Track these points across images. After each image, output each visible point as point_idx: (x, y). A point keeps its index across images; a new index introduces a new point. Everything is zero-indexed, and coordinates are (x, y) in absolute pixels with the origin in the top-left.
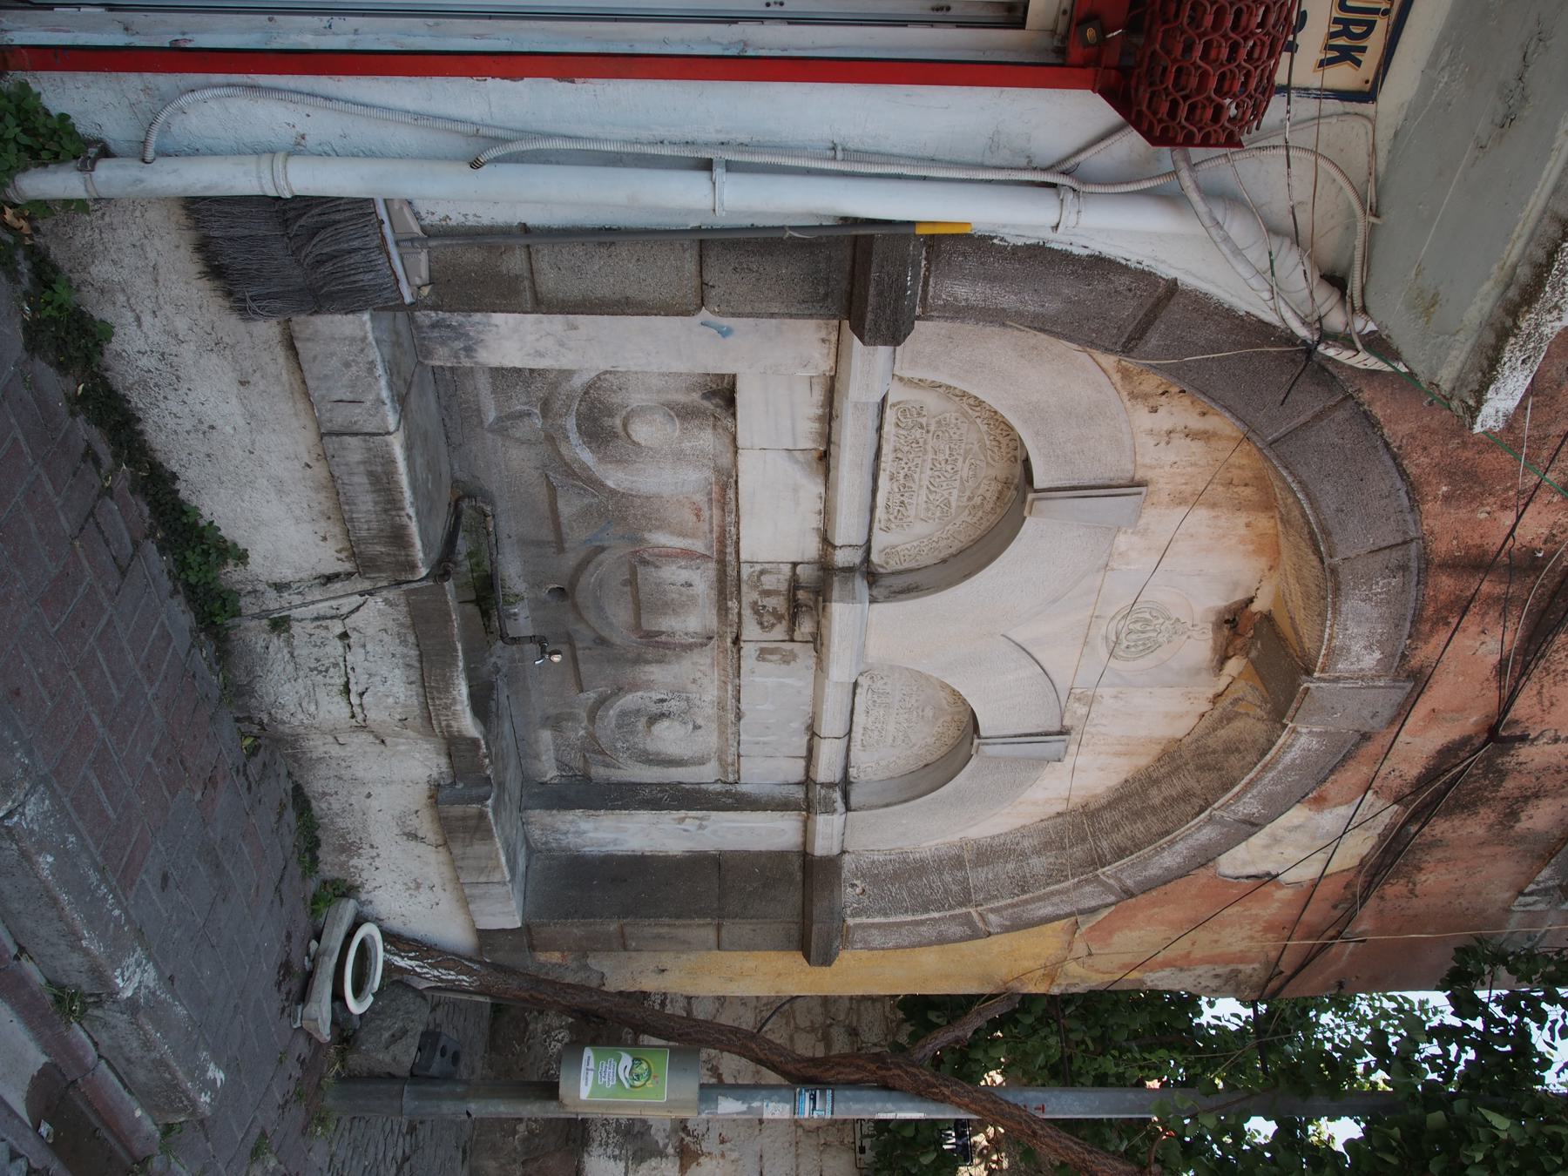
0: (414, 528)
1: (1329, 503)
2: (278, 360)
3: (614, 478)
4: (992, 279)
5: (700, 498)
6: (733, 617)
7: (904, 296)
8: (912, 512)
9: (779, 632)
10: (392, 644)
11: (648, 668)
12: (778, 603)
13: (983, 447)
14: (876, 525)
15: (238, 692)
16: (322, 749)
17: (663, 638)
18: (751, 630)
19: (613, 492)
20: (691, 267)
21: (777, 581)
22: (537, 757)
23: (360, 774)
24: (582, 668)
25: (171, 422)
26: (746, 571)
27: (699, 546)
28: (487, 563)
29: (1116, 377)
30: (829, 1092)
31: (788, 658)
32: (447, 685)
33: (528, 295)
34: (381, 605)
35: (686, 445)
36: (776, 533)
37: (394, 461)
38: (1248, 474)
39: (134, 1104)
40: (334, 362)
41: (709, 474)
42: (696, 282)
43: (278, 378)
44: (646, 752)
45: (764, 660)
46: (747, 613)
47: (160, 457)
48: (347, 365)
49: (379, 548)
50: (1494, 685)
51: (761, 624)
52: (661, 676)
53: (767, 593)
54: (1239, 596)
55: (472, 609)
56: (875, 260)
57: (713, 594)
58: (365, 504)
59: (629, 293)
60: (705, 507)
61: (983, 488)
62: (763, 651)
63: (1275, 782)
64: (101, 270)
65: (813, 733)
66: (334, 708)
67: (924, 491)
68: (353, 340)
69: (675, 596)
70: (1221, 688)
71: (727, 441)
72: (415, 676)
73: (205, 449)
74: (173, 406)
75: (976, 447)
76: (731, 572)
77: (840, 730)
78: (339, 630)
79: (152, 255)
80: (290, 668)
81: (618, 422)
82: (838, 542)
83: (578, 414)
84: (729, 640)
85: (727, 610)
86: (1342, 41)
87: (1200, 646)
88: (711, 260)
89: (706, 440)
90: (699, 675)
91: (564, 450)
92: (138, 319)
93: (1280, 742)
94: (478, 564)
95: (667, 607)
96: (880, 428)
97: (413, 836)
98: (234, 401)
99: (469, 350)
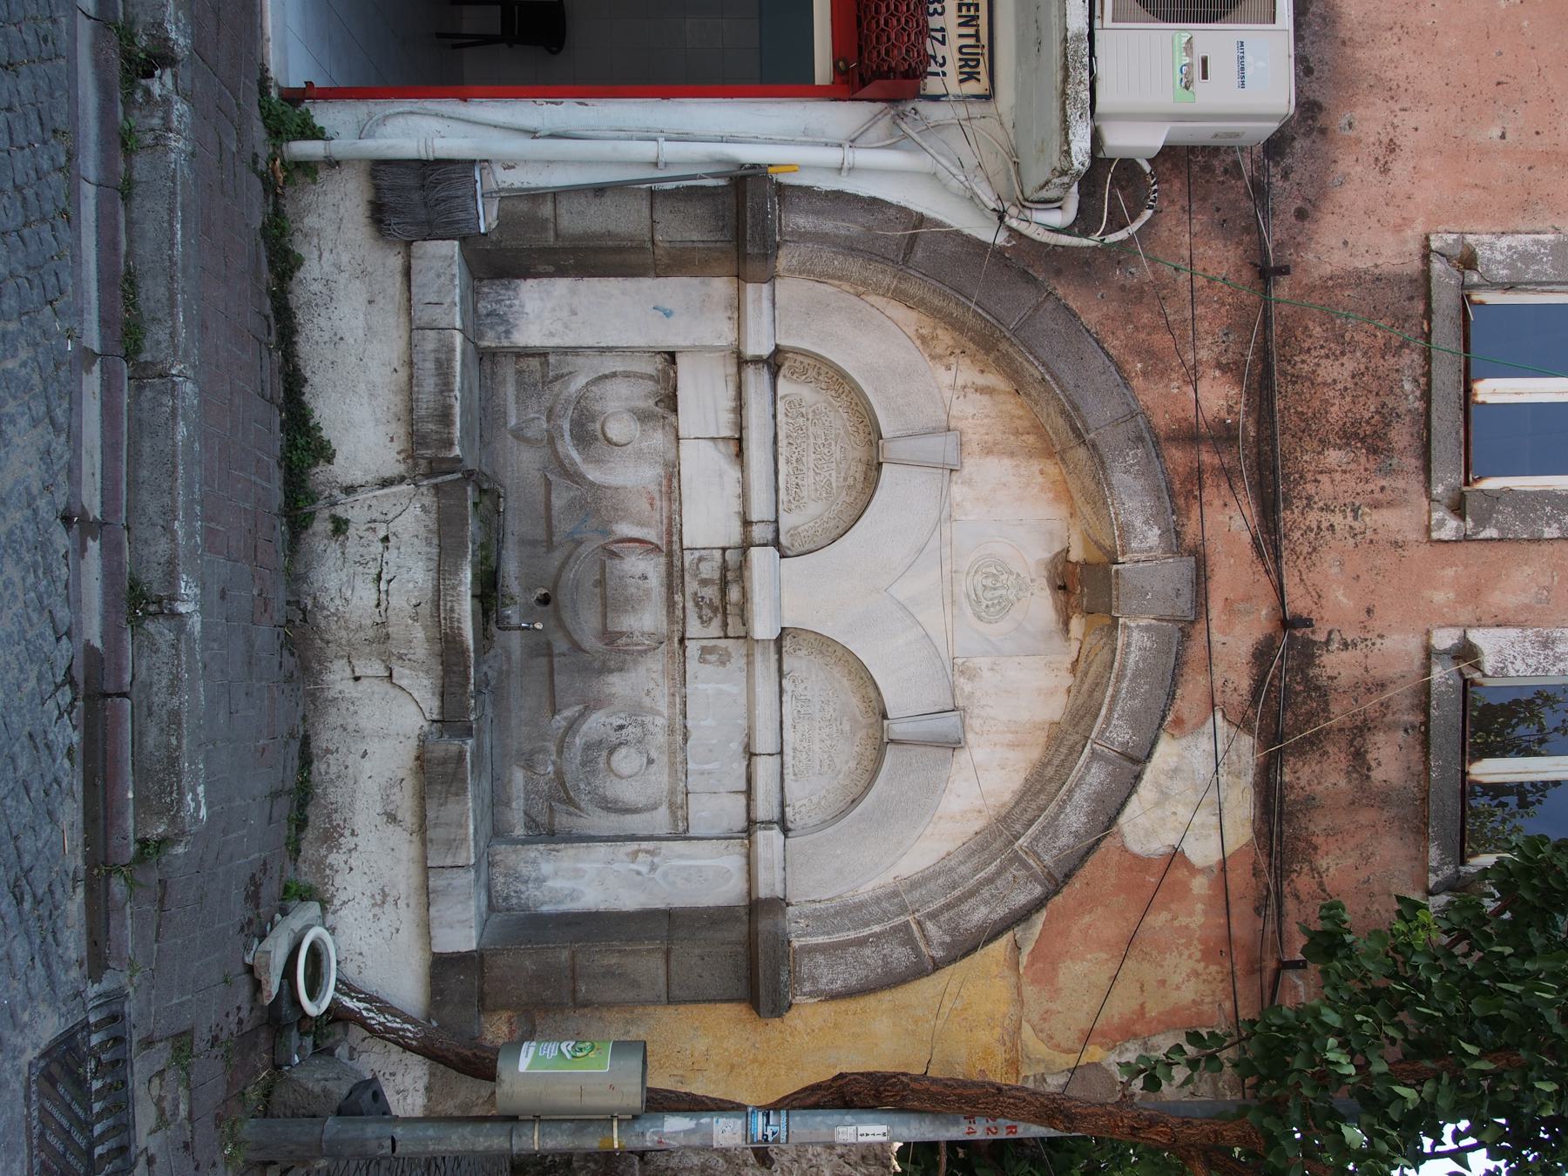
1: (1068, 379)
2: (395, 285)
3: (593, 474)
4: (817, 213)
5: (653, 488)
6: (679, 613)
7: (765, 218)
8: (805, 494)
10: (420, 546)
12: (711, 593)
13: (847, 432)
14: (781, 507)
15: (296, 576)
16: (339, 687)
18: (694, 628)
19: (592, 484)
20: (646, 212)
22: (508, 804)
23: (363, 723)
24: (556, 678)
25: (316, 333)
26: (688, 558)
27: (651, 534)
28: (493, 558)
29: (918, 342)
30: (783, 1112)
32: (457, 570)
33: (552, 233)
34: (418, 511)
36: (708, 523)
37: (454, 350)
38: (1027, 424)
40: (432, 274)
41: (660, 470)
42: (649, 222)
43: (392, 298)
44: (604, 798)
46: (690, 605)
47: (301, 363)
48: (439, 276)
49: (431, 426)
50: (1260, 568)
51: (700, 617)
52: (618, 685)
53: (704, 583)
54: (1057, 548)
56: (749, 195)
57: (664, 590)
58: (429, 384)
59: (611, 228)
60: (657, 496)
62: (704, 650)
63: (1132, 694)
64: (311, 221)
65: (750, 755)
66: (365, 594)
67: (812, 473)
68: (446, 257)
69: (634, 590)
70: (1075, 655)
72: (433, 565)
73: (331, 357)
74: (323, 322)
76: (677, 563)
78: (382, 534)
79: (342, 210)
80: (339, 563)
81: (598, 426)
82: (754, 518)
86: (967, 70)
87: (1041, 605)
88: (657, 206)
89: (658, 439)
90: (652, 685)
91: (560, 449)
92: (320, 257)
93: (1120, 643)
95: (630, 604)
96: (775, 416)
97: (392, 818)
98: (361, 317)
99: (508, 332)
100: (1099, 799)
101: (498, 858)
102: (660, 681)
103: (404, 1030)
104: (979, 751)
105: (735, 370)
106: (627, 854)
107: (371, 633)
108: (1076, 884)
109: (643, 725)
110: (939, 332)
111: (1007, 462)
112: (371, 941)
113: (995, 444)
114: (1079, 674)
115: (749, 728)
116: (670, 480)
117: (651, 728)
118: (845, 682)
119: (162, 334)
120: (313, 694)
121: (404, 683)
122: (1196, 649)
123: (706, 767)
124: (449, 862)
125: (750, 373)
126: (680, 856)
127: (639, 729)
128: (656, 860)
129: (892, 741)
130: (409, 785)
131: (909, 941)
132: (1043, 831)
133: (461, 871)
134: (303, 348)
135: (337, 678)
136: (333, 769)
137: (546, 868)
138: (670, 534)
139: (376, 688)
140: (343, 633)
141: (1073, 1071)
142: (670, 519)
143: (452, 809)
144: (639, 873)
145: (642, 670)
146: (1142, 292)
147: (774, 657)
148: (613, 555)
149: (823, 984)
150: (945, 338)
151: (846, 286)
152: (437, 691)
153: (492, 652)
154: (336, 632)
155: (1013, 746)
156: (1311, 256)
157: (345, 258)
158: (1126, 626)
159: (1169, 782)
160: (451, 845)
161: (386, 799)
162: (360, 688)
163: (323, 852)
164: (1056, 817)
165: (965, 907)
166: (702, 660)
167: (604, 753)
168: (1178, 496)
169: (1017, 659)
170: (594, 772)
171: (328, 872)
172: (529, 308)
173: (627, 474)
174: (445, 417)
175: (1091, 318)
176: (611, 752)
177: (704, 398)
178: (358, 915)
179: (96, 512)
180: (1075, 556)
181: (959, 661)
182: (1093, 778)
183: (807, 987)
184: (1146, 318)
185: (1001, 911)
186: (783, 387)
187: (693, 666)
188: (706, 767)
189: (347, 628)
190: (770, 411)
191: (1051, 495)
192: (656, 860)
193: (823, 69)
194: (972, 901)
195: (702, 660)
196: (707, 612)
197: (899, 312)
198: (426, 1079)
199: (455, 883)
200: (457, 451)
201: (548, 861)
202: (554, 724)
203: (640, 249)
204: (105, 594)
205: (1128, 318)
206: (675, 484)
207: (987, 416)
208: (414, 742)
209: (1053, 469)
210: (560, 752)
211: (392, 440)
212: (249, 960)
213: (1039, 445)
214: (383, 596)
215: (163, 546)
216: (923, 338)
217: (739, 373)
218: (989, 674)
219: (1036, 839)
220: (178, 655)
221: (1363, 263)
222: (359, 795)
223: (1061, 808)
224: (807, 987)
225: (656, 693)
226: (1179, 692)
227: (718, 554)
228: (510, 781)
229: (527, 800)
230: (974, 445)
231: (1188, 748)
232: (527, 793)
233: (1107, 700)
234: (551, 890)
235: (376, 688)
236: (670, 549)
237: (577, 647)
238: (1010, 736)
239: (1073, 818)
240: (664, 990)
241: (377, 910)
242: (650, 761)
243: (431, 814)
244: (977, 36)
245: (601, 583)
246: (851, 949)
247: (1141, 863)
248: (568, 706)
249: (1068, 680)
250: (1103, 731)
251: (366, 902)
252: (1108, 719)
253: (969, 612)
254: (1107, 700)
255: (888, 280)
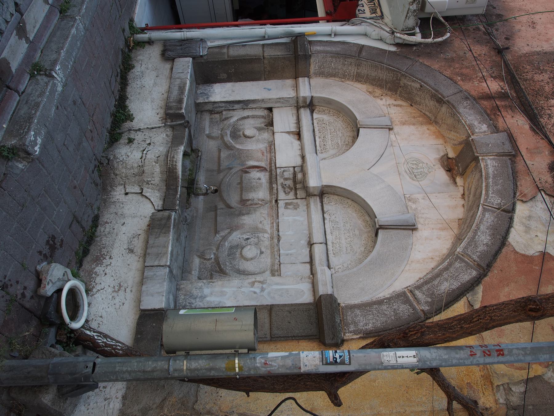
0: (185, 99)
1: (431, 83)
4: (324, 46)
5: (264, 149)
6: (275, 191)
8: (328, 147)
9: (291, 195)
11: (243, 217)
12: (290, 183)
13: (343, 128)
16: (118, 197)
17: (250, 202)
18: (282, 195)
21: (289, 174)
22: (190, 272)
24: (218, 218)
26: (278, 171)
27: (262, 164)
29: (368, 93)
31: (296, 207)
34: (164, 136)
35: (260, 137)
39: (7, 122)
45: (287, 208)
46: (280, 187)
51: (285, 192)
52: (247, 220)
53: (286, 179)
55: (185, 190)
57: (268, 185)
58: (175, 93)
60: (265, 152)
61: (347, 139)
63: (495, 183)
67: (330, 141)
71: (271, 134)
75: (341, 128)
76: (274, 173)
77: (322, 240)
83: (231, 132)
84: (274, 201)
85: (273, 188)
87: (442, 175)
89: (266, 135)
93: (482, 166)
94: (191, 174)
95: (252, 189)
96: (313, 124)
98: (153, 81)
100: (494, 229)
101: (182, 286)
102: (266, 218)
103: (116, 345)
104: (423, 232)
105: (296, 112)
106: (249, 283)
107: (136, 171)
108: (495, 272)
109: (258, 237)
110: (376, 90)
111: (412, 127)
112: (108, 310)
113: (406, 121)
114: (466, 198)
115: (310, 234)
116: (271, 147)
117: (262, 238)
118: (354, 215)
119: (76, 9)
120: (106, 200)
121: (147, 195)
122: (520, 166)
123: (290, 252)
124: (156, 263)
125: (302, 111)
126: (277, 284)
127: (256, 239)
128: (264, 286)
129: (382, 227)
130: (142, 238)
131: (407, 301)
132: (469, 244)
133: (161, 268)
134: (129, 89)
135: (118, 193)
136: (107, 230)
137: (206, 291)
138: (270, 164)
139: (134, 198)
140: (124, 170)
141: (527, 381)
142: (271, 159)
143: (162, 239)
144: (255, 293)
145: (258, 213)
146: (453, 59)
147: (319, 204)
148: (247, 172)
149: (361, 326)
150: (378, 92)
151: (337, 79)
152: (162, 198)
153: (190, 209)
154: (122, 170)
155: (442, 229)
156: (516, 49)
157: (150, 66)
158: (483, 159)
159: (528, 222)
160: (158, 256)
161: (130, 242)
162: (127, 198)
163: (93, 266)
164: (474, 237)
165: (436, 282)
166: (286, 208)
167: (239, 250)
168: (491, 116)
169: (434, 194)
170: (234, 259)
171: (94, 275)
172: (216, 91)
173: (254, 147)
174: (180, 101)
175: (436, 66)
176: (243, 248)
177: (284, 120)
178: (104, 297)
179: (31, 39)
180: (451, 155)
181: (407, 196)
182: (487, 220)
183: (352, 328)
184: (457, 66)
185: (456, 285)
186: (315, 116)
187: (281, 210)
188: (290, 252)
189: (126, 168)
190: (311, 122)
191: (434, 137)
192: (264, 286)
193: (321, 12)
194: (438, 279)
195: (286, 208)
196: (287, 190)
197: (359, 85)
198: (124, 391)
199: (158, 274)
200: (183, 111)
201: (208, 288)
202: (216, 239)
203: (259, 59)
204: (24, 59)
205: (450, 66)
206: (273, 147)
207: (401, 113)
208: (148, 219)
209: (432, 128)
210: (218, 249)
211: (158, 114)
212: (39, 268)
213: (425, 121)
214: (144, 155)
215: (54, 56)
216: (370, 92)
217: (298, 112)
218: (423, 201)
219: (466, 248)
220: (47, 86)
221: (538, 49)
222: (117, 241)
223: (475, 233)
224: (352, 328)
225: (265, 222)
226: (518, 184)
227: (292, 169)
228: (192, 262)
229: (199, 272)
230: (397, 122)
231: (532, 207)
232: (200, 269)
233: (484, 188)
234: (208, 302)
235: (134, 198)
236: (271, 170)
237: (229, 207)
238: (440, 226)
239: (483, 238)
240: (268, 332)
241: (115, 294)
242: (262, 253)
243: (151, 242)
244: (374, 4)
245: (241, 183)
246: (375, 306)
247: (527, 259)
248: (223, 230)
249: (462, 202)
250: (486, 200)
251: (110, 290)
252: (487, 194)
253: (408, 177)
254: (484, 188)
255: (353, 70)
